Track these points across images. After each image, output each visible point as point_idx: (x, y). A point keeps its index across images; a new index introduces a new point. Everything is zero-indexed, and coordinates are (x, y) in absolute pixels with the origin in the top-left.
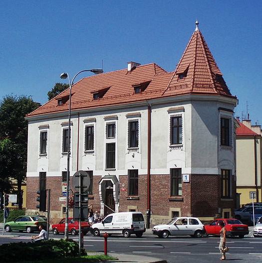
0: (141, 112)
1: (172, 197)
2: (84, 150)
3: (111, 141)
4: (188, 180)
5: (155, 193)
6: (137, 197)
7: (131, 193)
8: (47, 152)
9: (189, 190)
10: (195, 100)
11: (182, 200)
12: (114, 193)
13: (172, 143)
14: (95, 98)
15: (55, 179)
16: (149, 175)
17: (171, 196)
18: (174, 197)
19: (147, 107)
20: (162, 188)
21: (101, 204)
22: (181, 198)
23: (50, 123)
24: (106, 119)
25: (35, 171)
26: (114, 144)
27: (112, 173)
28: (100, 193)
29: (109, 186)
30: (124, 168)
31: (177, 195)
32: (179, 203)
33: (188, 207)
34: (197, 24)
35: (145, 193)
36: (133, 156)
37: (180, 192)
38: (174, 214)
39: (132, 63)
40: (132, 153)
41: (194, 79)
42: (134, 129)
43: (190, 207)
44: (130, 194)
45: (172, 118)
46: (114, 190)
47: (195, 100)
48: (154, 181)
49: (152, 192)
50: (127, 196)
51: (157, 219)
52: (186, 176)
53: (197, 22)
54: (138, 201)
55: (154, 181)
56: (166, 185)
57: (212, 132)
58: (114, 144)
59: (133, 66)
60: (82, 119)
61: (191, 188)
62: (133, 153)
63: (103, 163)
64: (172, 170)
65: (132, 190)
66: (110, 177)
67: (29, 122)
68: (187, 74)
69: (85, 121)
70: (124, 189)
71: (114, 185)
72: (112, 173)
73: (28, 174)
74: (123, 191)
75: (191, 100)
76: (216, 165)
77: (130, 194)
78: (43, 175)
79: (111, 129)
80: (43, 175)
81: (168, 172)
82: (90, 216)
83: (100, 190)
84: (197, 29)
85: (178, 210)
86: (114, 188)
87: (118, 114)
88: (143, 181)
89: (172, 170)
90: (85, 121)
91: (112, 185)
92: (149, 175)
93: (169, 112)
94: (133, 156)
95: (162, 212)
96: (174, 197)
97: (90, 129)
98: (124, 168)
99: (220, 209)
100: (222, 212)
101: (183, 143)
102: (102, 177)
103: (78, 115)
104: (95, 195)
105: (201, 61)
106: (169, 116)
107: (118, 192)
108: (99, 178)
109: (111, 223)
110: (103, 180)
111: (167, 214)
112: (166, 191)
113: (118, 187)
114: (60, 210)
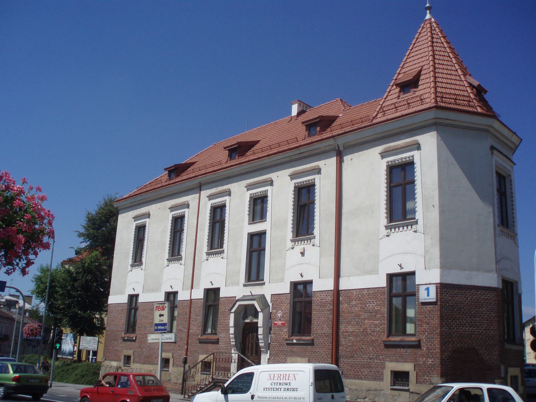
0: (321, 164)
1: (392, 339)
2: (205, 249)
3: (257, 228)
4: (433, 296)
5: (350, 329)
6: (307, 338)
7: (296, 329)
8: (144, 260)
9: (436, 321)
10: (441, 124)
11: (418, 346)
12: (260, 331)
13: (391, 217)
14: (231, 156)
15: (150, 306)
16: (337, 292)
17: (389, 336)
18: (398, 339)
19: (335, 153)
20: (369, 319)
21: (233, 351)
22: (413, 339)
23: (152, 209)
24: (249, 187)
25: (122, 293)
26: (262, 235)
27: (257, 291)
28: (232, 331)
29: (250, 317)
30: (282, 280)
31: (404, 332)
32: (409, 350)
33: (434, 361)
34: (429, 8)
35: (327, 330)
36: (303, 254)
37: (410, 328)
38: (205, 365)
39: (300, 103)
40: (299, 247)
41: (436, 89)
42: (304, 200)
43: (438, 361)
44: (293, 334)
45: (391, 169)
46: (260, 324)
47: (441, 124)
48: (349, 302)
49: (342, 328)
50: (287, 337)
51: (354, 387)
52: (428, 289)
53: (428, 5)
54: (309, 347)
55: (349, 302)
56: (376, 312)
57: (483, 198)
58: (262, 235)
59: (301, 109)
60: (205, 193)
61: (441, 317)
62: (302, 247)
63: (239, 271)
64: (391, 277)
65: (297, 326)
66: (252, 298)
67: (120, 212)
68: (420, 83)
69: (211, 197)
70: (279, 323)
71: (261, 315)
72: (257, 291)
73: (112, 299)
74: (279, 326)
75: (436, 124)
76: (493, 266)
77: (293, 334)
78: (133, 298)
79: (258, 207)
80: (133, 298)
81: (382, 283)
82: (77, 399)
83: (232, 323)
84: (428, 16)
85: (407, 367)
86: (260, 321)
87: (273, 176)
88: (323, 305)
89: (391, 277)
90: (211, 197)
91: (256, 316)
92: (337, 292)
93: (383, 155)
94: (303, 254)
95: (366, 371)
96: (398, 339)
97: (219, 210)
98: (282, 280)
99: (502, 367)
100: (506, 373)
101: (419, 216)
102: (237, 299)
103: (199, 188)
104: (221, 335)
105: (445, 63)
106: (382, 165)
107: (269, 330)
108: (233, 301)
109: (248, 395)
110: (238, 303)
111: (379, 377)
112: (376, 326)
113: (269, 317)
114: (157, 364)
